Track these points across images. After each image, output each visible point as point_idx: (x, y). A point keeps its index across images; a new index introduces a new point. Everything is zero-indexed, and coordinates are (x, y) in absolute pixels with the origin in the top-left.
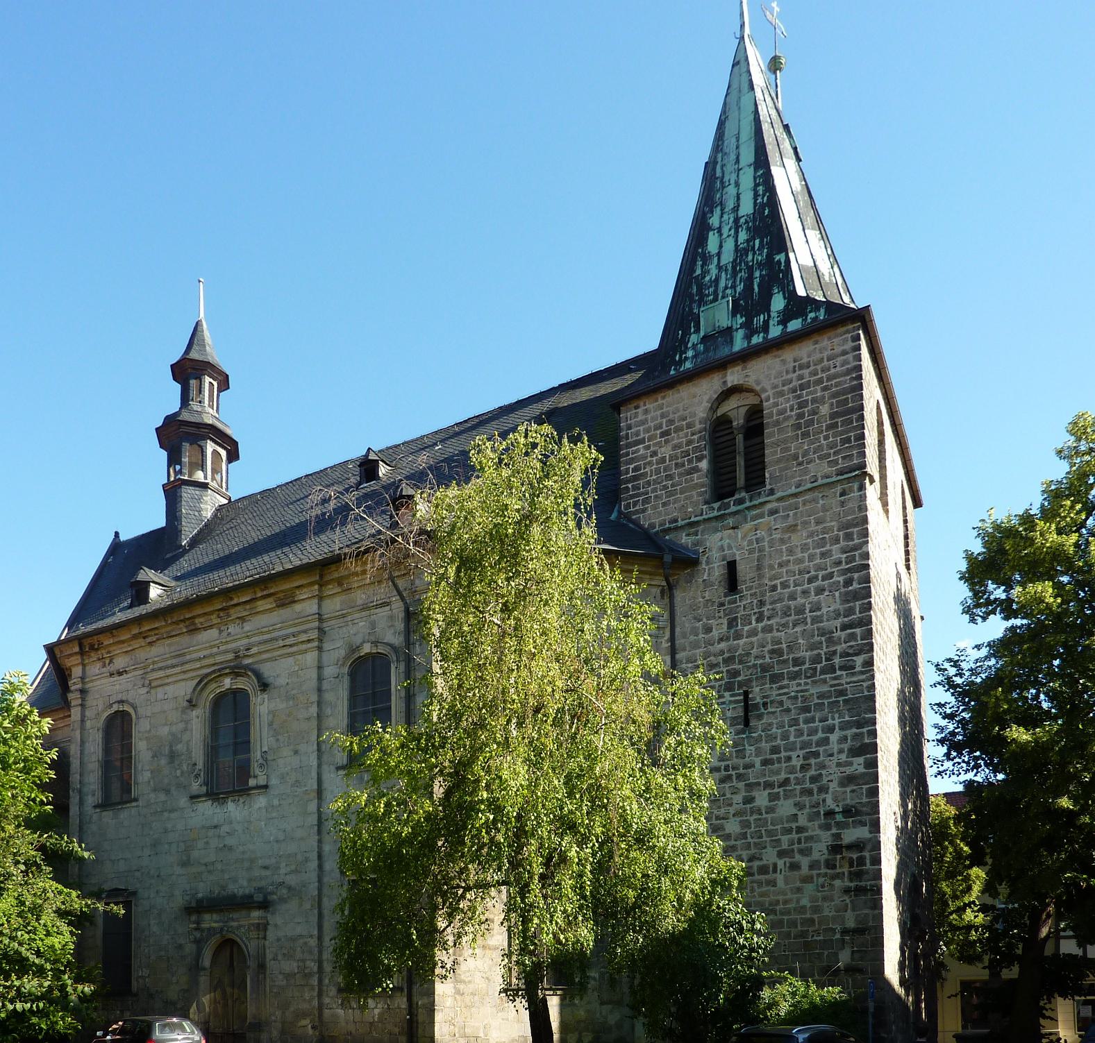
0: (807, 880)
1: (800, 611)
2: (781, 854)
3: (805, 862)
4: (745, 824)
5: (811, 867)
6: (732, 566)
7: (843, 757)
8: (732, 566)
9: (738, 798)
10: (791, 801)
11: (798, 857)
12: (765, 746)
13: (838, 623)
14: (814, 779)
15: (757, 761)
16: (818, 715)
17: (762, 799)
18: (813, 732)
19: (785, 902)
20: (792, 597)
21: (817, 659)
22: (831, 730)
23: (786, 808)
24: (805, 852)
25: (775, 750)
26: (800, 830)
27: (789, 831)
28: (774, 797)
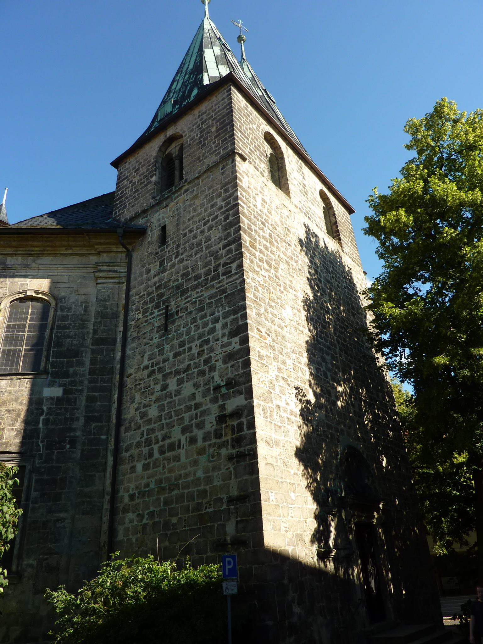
0: (201, 452)
1: (199, 244)
2: (184, 430)
3: (199, 434)
4: (161, 408)
5: (205, 439)
6: (164, 229)
7: (225, 339)
8: (164, 229)
9: (158, 387)
10: (191, 383)
11: (195, 431)
12: (176, 342)
13: (221, 245)
14: (206, 362)
15: (171, 355)
16: (209, 312)
17: (173, 386)
18: (205, 325)
19: (186, 475)
20: (195, 237)
21: (208, 273)
22: (217, 320)
23: (188, 389)
24: (200, 426)
25: (182, 344)
26: (197, 406)
27: (189, 409)
28: (180, 382)
